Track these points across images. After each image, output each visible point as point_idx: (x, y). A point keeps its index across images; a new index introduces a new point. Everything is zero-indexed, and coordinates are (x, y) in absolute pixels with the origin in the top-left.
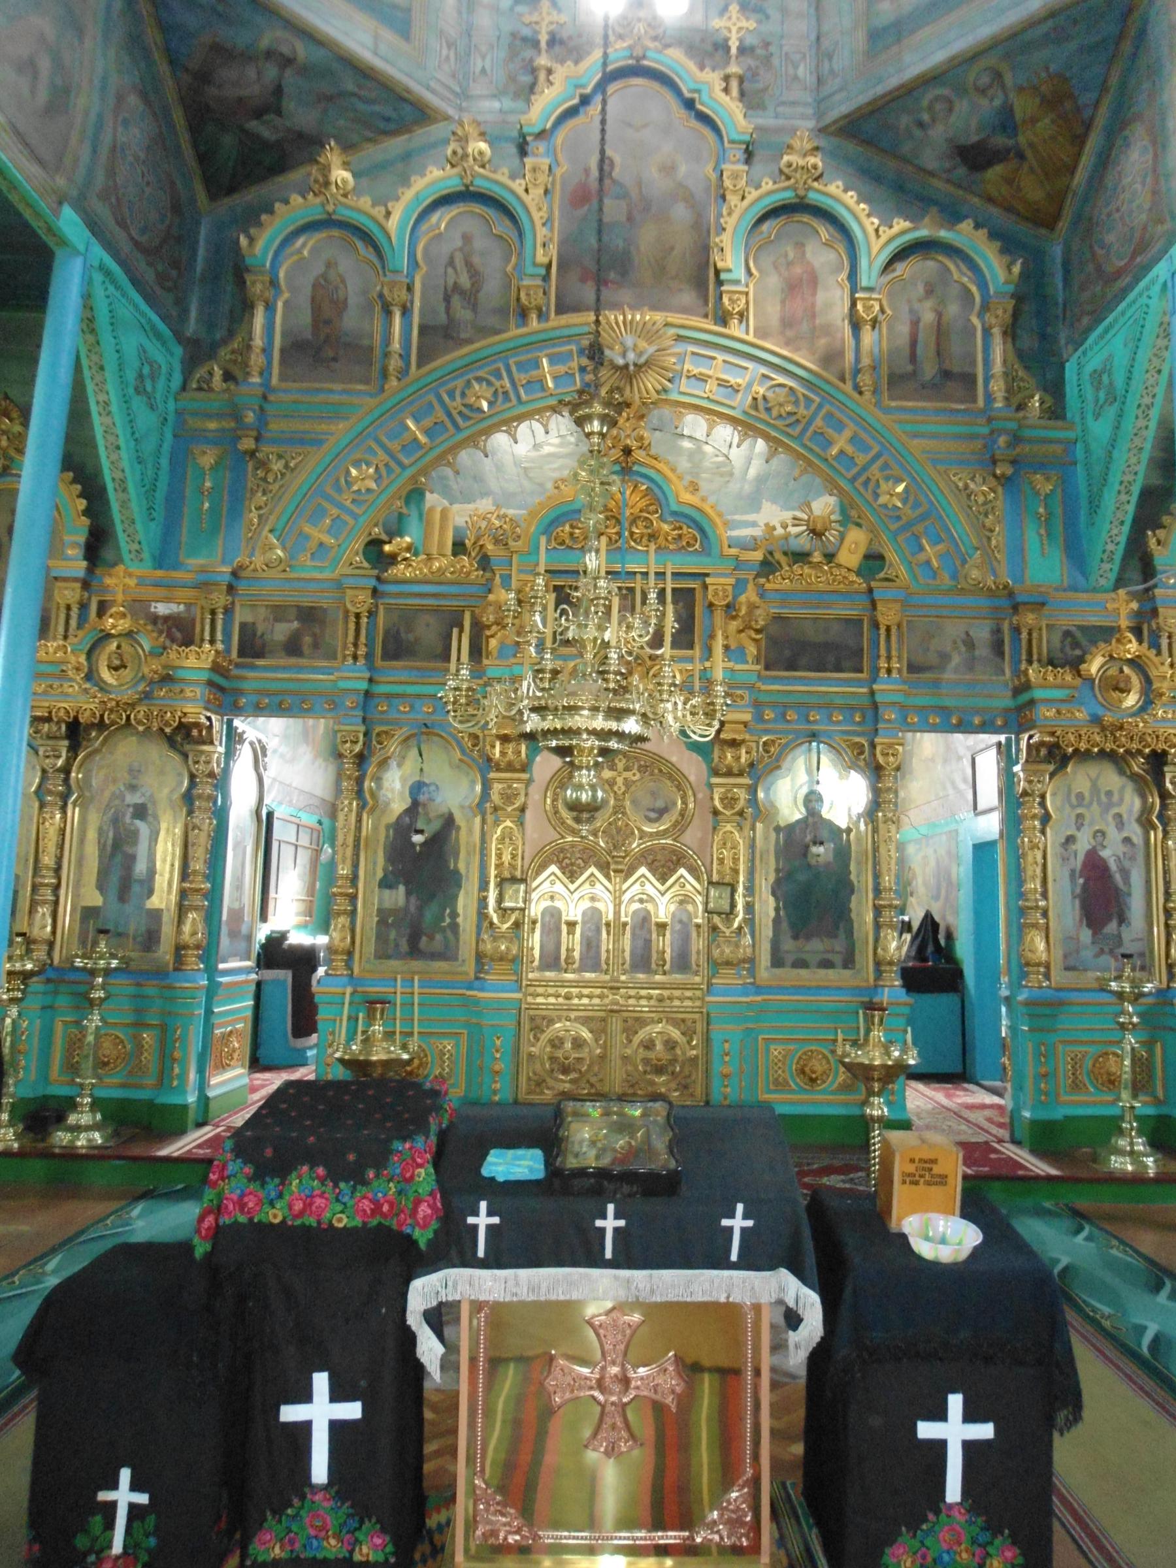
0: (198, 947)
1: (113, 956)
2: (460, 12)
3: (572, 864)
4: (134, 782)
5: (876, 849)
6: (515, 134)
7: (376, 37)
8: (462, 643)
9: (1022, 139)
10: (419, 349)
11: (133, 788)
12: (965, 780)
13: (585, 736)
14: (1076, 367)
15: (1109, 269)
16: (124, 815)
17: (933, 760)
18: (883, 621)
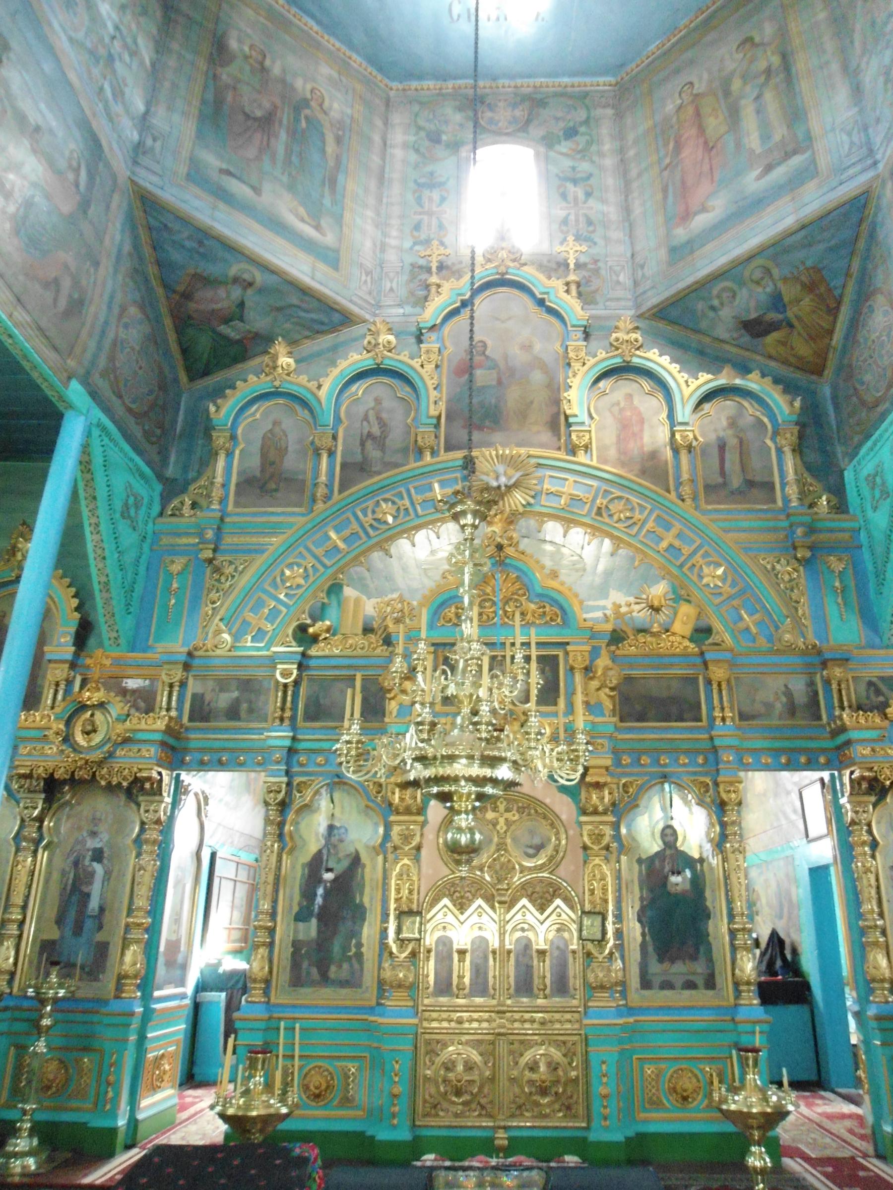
0: (136, 977)
1: (61, 986)
2: (374, 252)
3: (462, 897)
4: (95, 829)
5: (727, 878)
6: (414, 329)
7: (314, 268)
8: (353, 702)
9: (790, 314)
10: (341, 480)
11: (94, 834)
12: (795, 811)
13: (463, 783)
14: (852, 473)
15: (869, 399)
16: (84, 857)
17: (765, 795)
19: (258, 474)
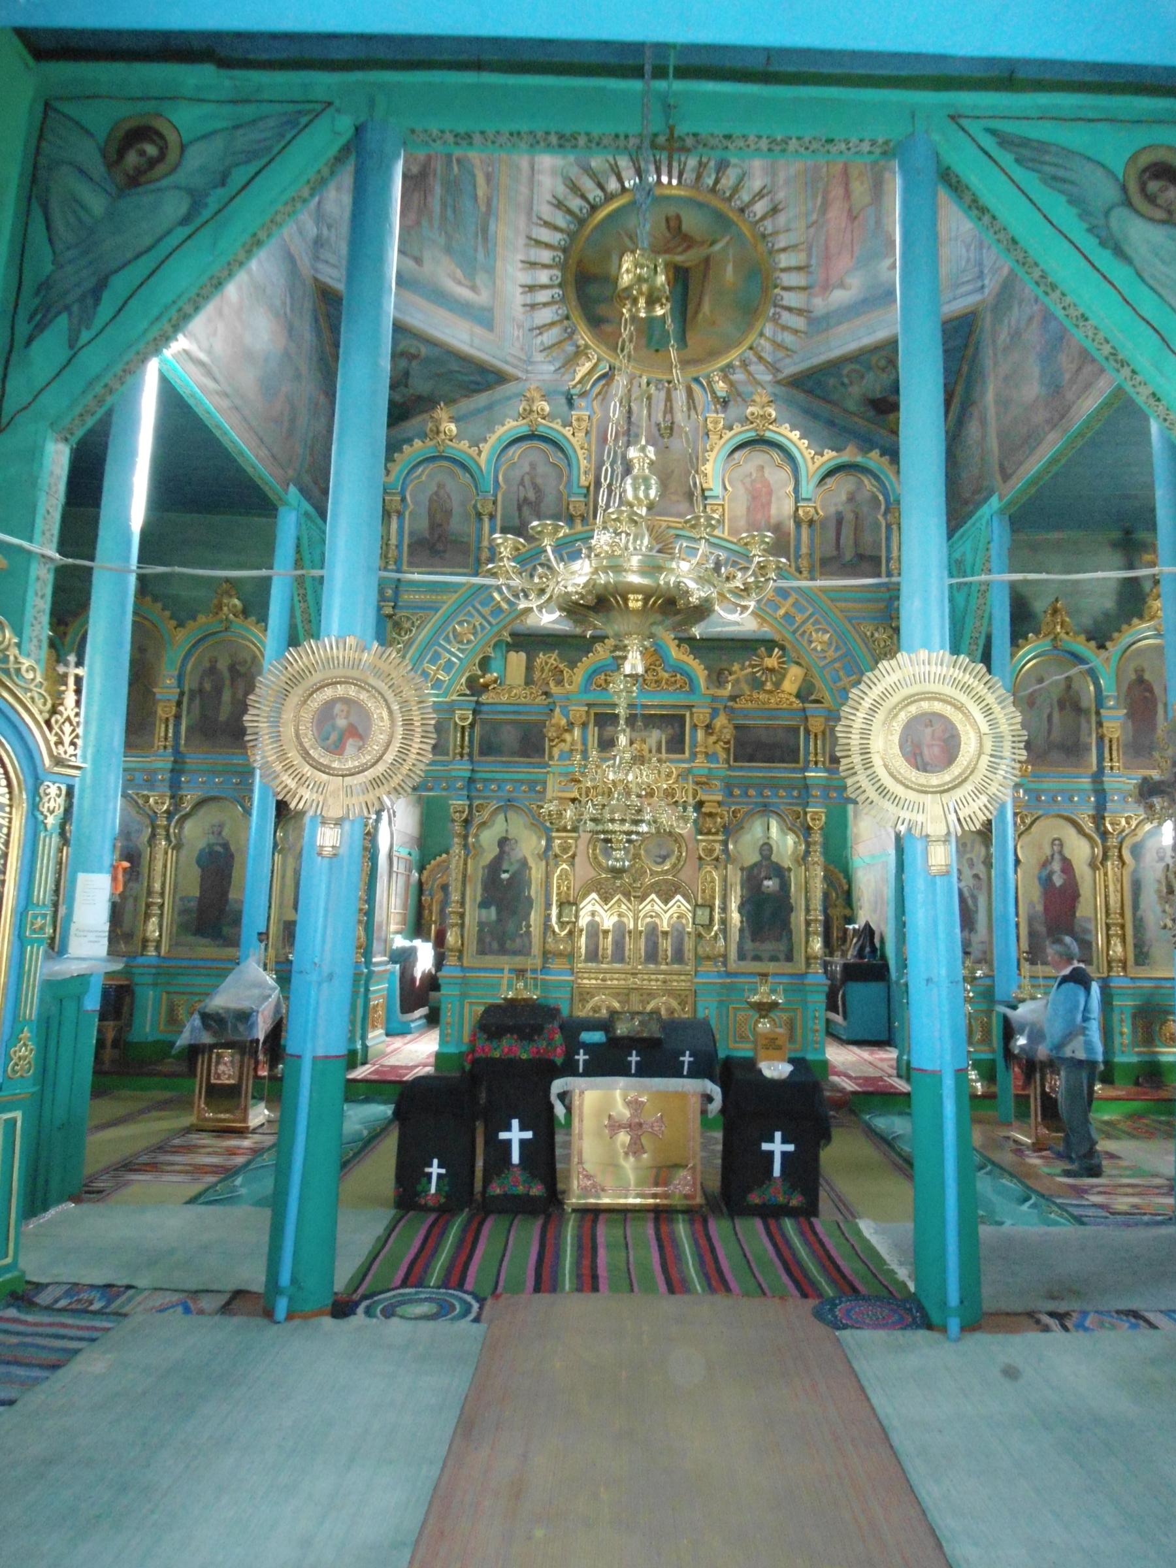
7: (472, 334)
18: (813, 729)
19: (427, 535)
